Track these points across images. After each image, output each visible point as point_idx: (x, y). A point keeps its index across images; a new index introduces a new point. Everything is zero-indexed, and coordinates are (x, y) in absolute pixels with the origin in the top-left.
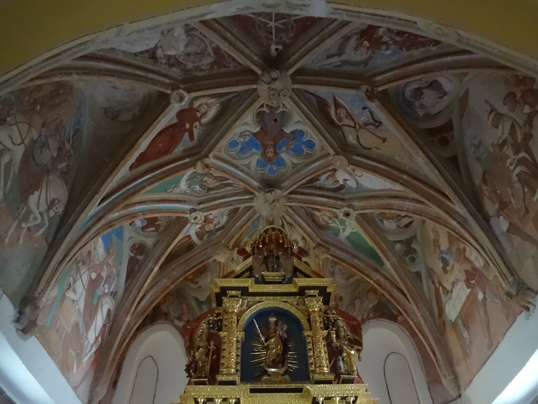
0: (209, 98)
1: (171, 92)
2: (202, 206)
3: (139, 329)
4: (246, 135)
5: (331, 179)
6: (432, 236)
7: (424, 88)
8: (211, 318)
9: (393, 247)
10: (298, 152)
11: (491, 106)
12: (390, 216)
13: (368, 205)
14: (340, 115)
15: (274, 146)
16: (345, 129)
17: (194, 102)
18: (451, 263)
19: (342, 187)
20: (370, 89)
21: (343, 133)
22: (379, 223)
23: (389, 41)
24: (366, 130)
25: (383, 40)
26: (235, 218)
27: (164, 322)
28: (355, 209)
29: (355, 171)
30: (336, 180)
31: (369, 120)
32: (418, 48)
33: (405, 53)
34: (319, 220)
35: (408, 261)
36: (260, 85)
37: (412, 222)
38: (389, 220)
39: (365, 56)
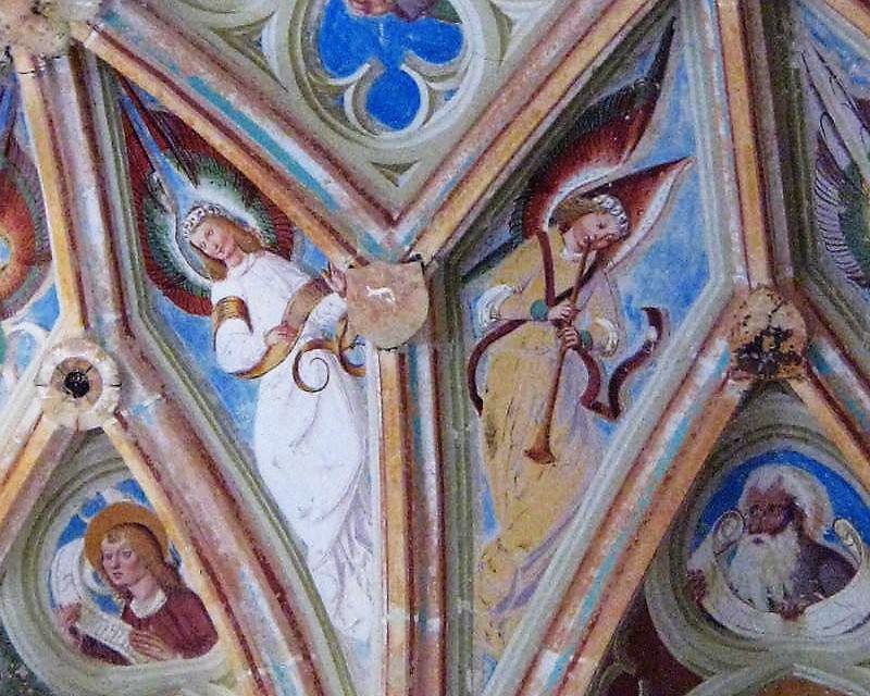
5: (217, 237)
7: (800, 530)
13: (171, 467)
16: (529, 252)
19: (193, 301)
20: (794, 345)
21: (506, 249)
22: (61, 524)
24: (554, 355)
28: (124, 414)
30: (221, 262)
37: (116, 658)
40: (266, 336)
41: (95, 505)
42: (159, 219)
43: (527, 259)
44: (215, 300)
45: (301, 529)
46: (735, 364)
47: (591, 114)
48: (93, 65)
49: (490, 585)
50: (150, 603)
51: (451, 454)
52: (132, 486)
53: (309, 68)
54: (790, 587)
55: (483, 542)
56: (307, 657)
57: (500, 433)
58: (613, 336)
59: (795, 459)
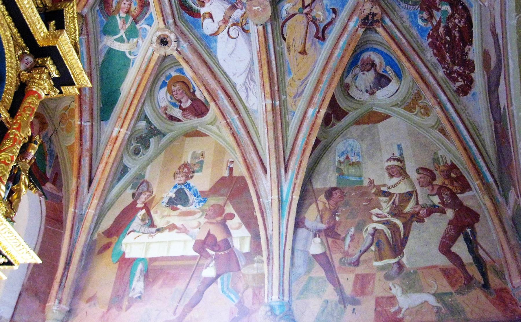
6: (188, 158)
11: (401, 155)
12: (174, 91)
18: (192, 208)
22: (160, 83)
23: (436, 20)
25: (435, 12)
28: (179, 49)
29: (235, 27)
31: (321, 22)
32: (436, 55)
33: (426, 43)
35: (132, 147)
37: (179, 120)
38: (170, 94)
40: (218, 23)
41: (169, 77)
44: (202, 13)
45: (234, 79)
46: (360, 24)
49: (291, 91)
50: (187, 103)
54: (372, 85)
55: (288, 79)
56: (240, 115)
57: (291, 47)
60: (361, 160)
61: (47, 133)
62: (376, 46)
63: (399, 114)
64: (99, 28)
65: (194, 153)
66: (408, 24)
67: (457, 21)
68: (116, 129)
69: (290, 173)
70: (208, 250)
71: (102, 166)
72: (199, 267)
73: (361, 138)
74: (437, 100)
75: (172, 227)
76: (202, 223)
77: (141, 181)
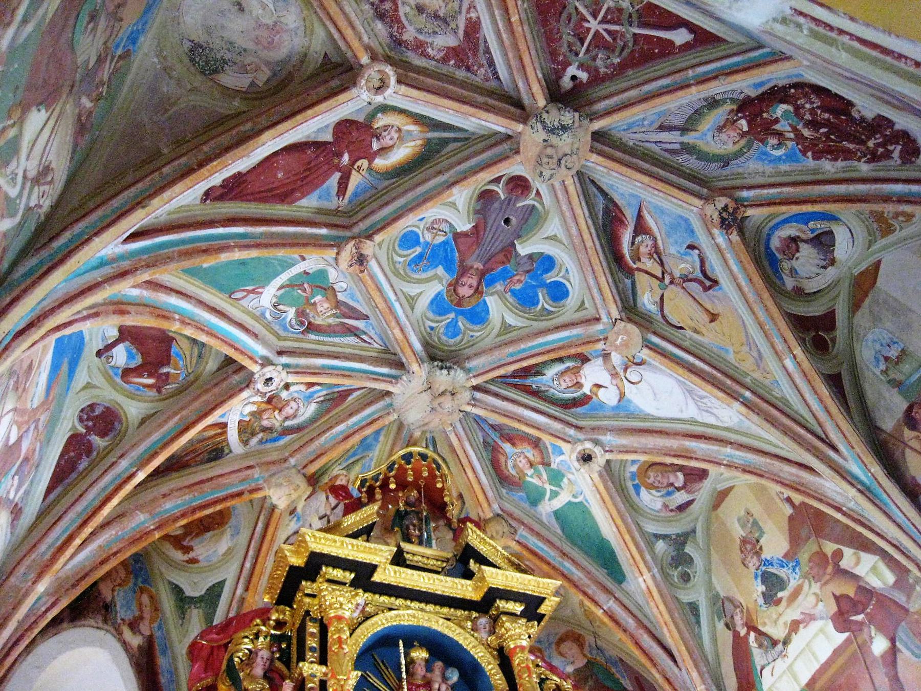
0: (409, 120)
1: (368, 61)
2: (284, 360)
3: (56, 622)
4: (440, 230)
5: (567, 379)
6: (738, 532)
7: (803, 241)
8: (264, 628)
9: (651, 545)
10: (525, 300)
13: (635, 445)
14: (638, 249)
15: (482, 274)
16: (641, 278)
17: (379, 115)
18: (793, 584)
19: (585, 400)
20: (731, 205)
21: (633, 284)
22: (632, 491)
25: (777, 127)
26: (334, 413)
27: (101, 625)
29: (629, 371)
31: (693, 273)
32: (836, 159)
33: (809, 162)
34: (506, 462)
35: (676, 580)
36: (532, 128)
37: (690, 503)
39: (730, 148)
42: (549, 394)
43: (642, 279)
44: (589, 393)
45: (685, 416)
47: (604, 226)
48: (484, 385)
49: (747, 365)
51: (692, 349)
52: (633, 462)
53: (529, 313)
55: (731, 357)
56: (731, 443)
58: (688, 266)
59: (776, 227)
60: (902, 346)
61: (590, 646)
62: (771, 224)
63: (884, 248)
64: (526, 505)
65: (739, 520)
66: (769, 169)
67: (808, 106)
68: (641, 580)
69: (842, 447)
70: (853, 618)
71: (665, 630)
72: (864, 648)
73: (876, 320)
74: (893, 202)
75: (795, 626)
76: (818, 591)
77: (720, 603)
